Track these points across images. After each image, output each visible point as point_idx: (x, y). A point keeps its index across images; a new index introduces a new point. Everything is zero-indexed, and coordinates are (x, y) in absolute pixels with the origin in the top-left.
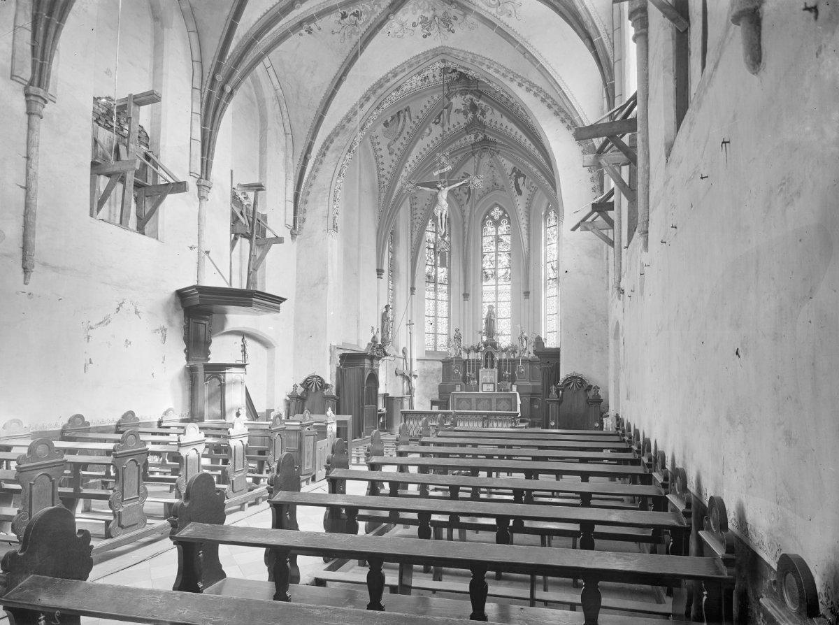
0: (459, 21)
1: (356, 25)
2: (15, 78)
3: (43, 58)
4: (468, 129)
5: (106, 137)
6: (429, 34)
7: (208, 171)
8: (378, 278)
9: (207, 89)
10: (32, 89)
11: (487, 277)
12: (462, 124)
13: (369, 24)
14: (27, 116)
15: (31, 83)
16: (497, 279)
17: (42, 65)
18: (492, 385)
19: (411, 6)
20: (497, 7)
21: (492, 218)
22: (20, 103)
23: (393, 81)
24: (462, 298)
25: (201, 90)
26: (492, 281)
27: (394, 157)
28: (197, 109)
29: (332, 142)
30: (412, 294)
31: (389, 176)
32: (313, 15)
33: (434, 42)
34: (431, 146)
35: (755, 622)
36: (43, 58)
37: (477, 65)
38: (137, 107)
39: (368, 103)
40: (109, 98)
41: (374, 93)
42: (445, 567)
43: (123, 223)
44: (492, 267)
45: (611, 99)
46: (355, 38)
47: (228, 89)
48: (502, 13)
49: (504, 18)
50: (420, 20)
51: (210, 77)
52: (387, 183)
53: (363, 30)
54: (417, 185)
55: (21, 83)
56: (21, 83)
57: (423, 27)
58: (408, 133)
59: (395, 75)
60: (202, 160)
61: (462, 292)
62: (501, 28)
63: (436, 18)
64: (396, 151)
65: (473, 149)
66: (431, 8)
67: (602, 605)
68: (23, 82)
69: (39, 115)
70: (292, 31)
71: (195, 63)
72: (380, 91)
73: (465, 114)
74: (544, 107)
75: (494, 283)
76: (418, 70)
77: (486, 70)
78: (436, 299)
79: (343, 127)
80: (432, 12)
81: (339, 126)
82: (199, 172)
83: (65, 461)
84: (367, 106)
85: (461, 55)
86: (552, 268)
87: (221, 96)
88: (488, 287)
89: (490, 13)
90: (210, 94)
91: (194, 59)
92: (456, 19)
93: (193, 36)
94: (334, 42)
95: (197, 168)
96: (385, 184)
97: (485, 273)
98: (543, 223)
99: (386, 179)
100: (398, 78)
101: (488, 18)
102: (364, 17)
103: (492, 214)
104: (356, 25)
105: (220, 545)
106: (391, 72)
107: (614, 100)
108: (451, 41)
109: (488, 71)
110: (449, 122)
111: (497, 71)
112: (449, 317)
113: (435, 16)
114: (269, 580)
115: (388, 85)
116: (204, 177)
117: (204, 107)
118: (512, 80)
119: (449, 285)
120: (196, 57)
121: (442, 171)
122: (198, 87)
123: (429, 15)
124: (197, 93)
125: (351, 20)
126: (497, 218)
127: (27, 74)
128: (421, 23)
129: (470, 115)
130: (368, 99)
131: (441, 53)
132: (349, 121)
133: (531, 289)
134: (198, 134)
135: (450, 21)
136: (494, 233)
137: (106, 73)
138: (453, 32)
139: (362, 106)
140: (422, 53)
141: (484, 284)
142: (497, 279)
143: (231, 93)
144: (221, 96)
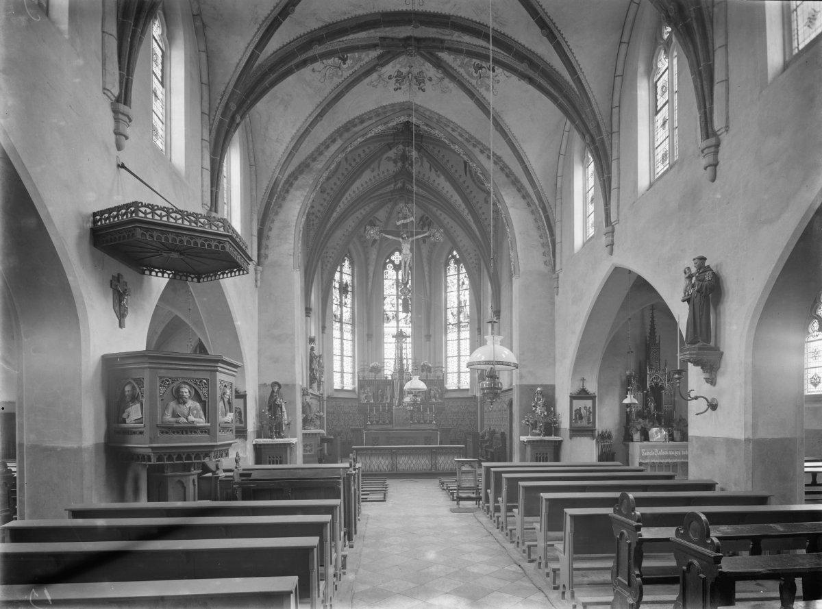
0: (434, 82)
1: (339, 67)
2: (105, 91)
4: (395, 177)
6: (400, 89)
8: (306, 316)
11: (388, 318)
12: (391, 172)
13: (353, 70)
16: (398, 321)
17: (127, 79)
21: (393, 262)
23: (360, 127)
24: (366, 338)
25: (209, 116)
26: (393, 323)
27: (325, 196)
28: (206, 137)
29: (296, 179)
30: (323, 333)
31: (319, 215)
33: (401, 97)
34: (361, 189)
36: (128, 75)
37: (442, 125)
39: (335, 145)
41: (341, 136)
44: (393, 309)
45: (607, 189)
46: (337, 80)
50: (396, 74)
51: (223, 103)
52: (316, 221)
53: (346, 74)
54: (381, 232)
56: (618, 206)
57: (397, 81)
58: (343, 174)
59: (362, 122)
60: (212, 191)
61: (365, 333)
62: (479, 100)
63: (410, 75)
64: (329, 191)
65: (392, 195)
66: (408, 65)
69: (124, 136)
71: (204, 86)
72: (346, 135)
73: (395, 162)
74: (504, 178)
75: (396, 325)
76: (385, 120)
77: (451, 132)
78: (459, 339)
79: (308, 166)
80: (408, 69)
81: (303, 163)
84: (334, 148)
85: (428, 113)
86: (452, 313)
88: (390, 329)
89: (471, 84)
90: (221, 122)
92: (430, 79)
93: (203, 55)
94: (314, 80)
95: (208, 199)
96: (315, 222)
97: (387, 315)
98: (443, 274)
99: (316, 217)
100: (365, 124)
103: (393, 258)
104: (339, 67)
105: (318, 538)
106: (358, 118)
107: (610, 193)
108: (419, 99)
109: (453, 133)
110: (379, 167)
111: (461, 136)
112: (353, 357)
113: (409, 73)
114: (806, 430)
115: (356, 129)
116: (213, 209)
117: (214, 134)
118: (474, 146)
119: (353, 325)
120: (205, 79)
121: (405, 221)
122: (207, 112)
123: (404, 71)
126: (397, 262)
127: (116, 91)
128: (396, 77)
129: (400, 164)
130: (334, 141)
131: (406, 108)
132: (314, 160)
133: (432, 333)
134: (207, 164)
135: (423, 81)
136: (395, 277)
138: (424, 90)
139: (328, 147)
140: (389, 105)
141: (385, 325)
142: (398, 321)
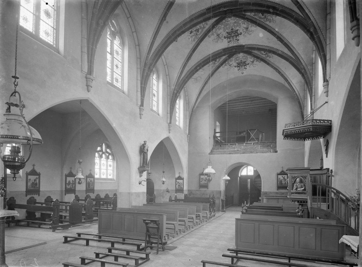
3: (91, 63)
9: (143, 68)
10: (88, 76)
14: (86, 87)
15: (88, 74)
18: (300, 228)
19: (223, 26)
20: (264, 19)
35: (68, 5)
36: (91, 63)
42: (68, 224)
49: (268, 23)
67: (67, 178)
71: (138, 59)
83: (8, 201)
91: (138, 57)
101: (297, 55)
102: (200, 30)
120: (138, 57)
124: (139, 70)
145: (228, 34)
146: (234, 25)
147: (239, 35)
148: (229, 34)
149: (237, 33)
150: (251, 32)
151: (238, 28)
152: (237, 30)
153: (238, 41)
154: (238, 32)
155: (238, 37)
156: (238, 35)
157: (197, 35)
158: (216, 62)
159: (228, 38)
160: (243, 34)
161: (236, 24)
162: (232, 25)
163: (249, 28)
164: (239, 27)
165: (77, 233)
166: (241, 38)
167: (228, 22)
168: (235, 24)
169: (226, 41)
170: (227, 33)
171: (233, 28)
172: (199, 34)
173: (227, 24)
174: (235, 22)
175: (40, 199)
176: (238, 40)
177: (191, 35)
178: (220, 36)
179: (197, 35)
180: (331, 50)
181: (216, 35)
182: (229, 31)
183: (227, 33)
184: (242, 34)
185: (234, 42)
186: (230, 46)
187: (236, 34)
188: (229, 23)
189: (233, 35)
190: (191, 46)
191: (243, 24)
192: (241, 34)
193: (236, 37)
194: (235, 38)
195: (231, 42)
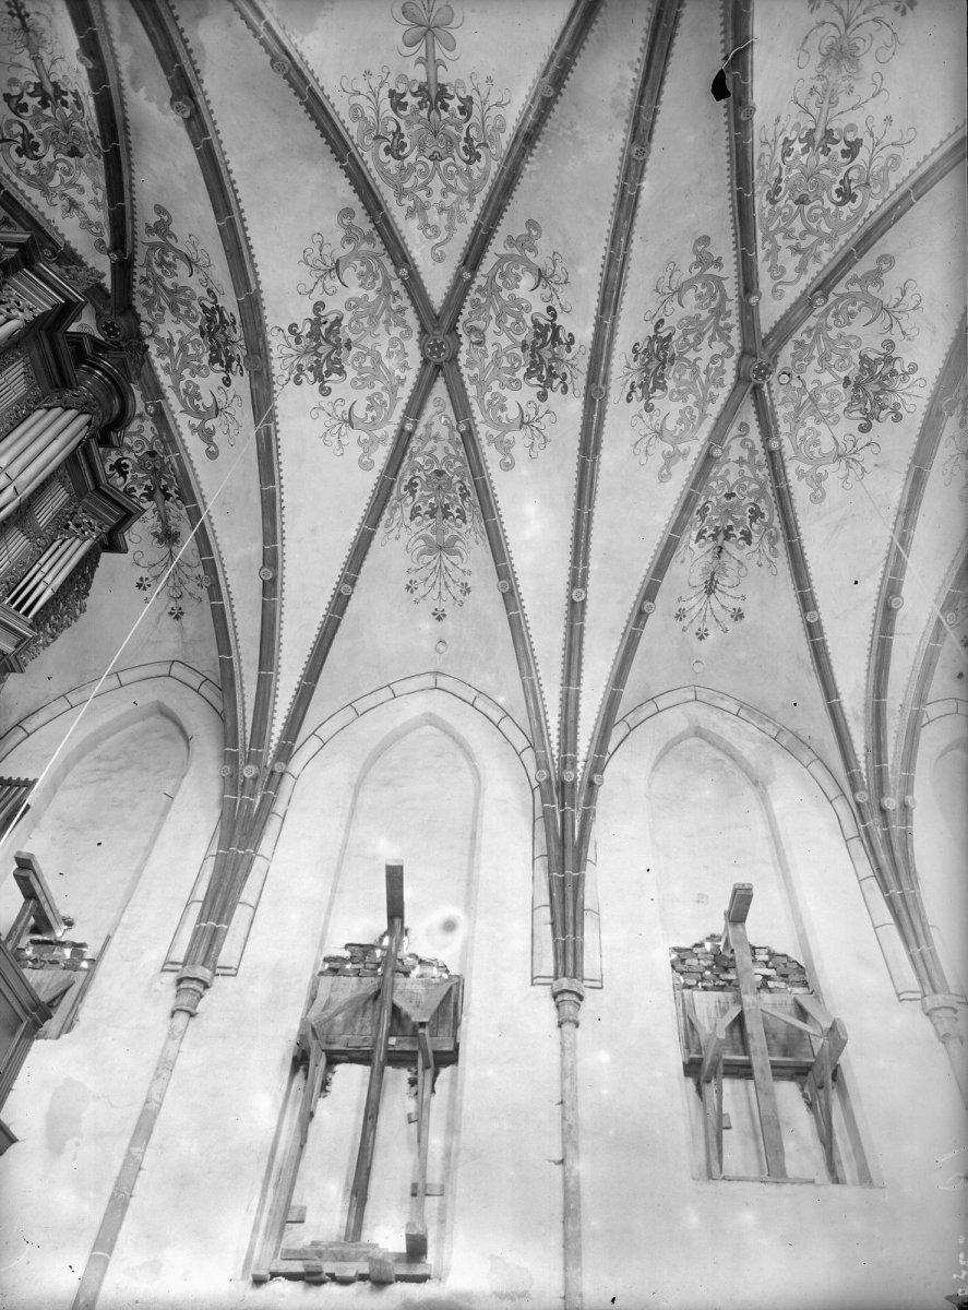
5: (712, 1006)
7: (579, 953)
22: (546, 1011)
32: (662, 579)
38: (739, 926)
40: (712, 938)
43: (773, 1169)
47: (891, 803)
48: (884, 182)
49: (894, 179)
55: (225, 968)
68: (547, 981)
70: (937, 642)
82: (913, 983)
87: (886, 823)
102: (392, 164)
116: (928, 990)
125: (758, 532)
137: (698, 902)
143: (905, 807)
144: (886, 823)
145: (332, 325)
146: (368, 354)
147: (318, 384)
148: (329, 331)
149: (328, 374)
150: (336, 445)
151: (351, 373)
152: (341, 372)
153: (291, 383)
154: (334, 376)
155: (311, 376)
156: (320, 377)
157: (377, 137)
158: (15, 156)
159: (316, 323)
160: (325, 401)
161: (368, 363)
162: (368, 342)
163: (354, 434)
164: (354, 381)
165: (947, 1298)
166: (309, 389)
167: (387, 322)
168: (368, 358)
169: (301, 312)
170: (338, 321)
171: (354, 350)
172: (376, 155)
173: (378, 317)
174: (380, 362)
175: (781, 1037)
176: (298, 382)
177: (384, 93)
178: (328, 282)
179: (377, 137)
180: (421, 693)
181: (340, 253)
182: (346, 333)
183: (338, 321)
184: (322, 398)
185: (289, 360)
186: (269, 338)
187: (325, 369)
188: (382, 327)
189: (324, 349)
190: (783, 562)
191: (369, 399)
192: (325, 392)
193: (310, 369)
194: (306, 361)
195: (292, 340)
